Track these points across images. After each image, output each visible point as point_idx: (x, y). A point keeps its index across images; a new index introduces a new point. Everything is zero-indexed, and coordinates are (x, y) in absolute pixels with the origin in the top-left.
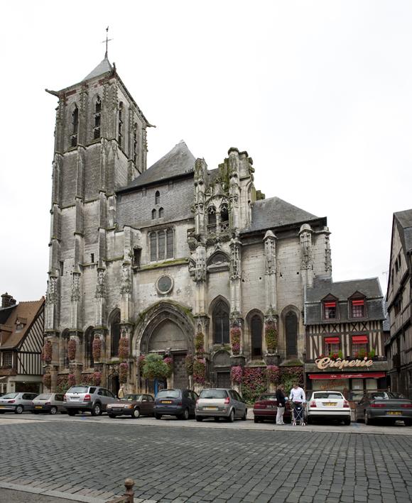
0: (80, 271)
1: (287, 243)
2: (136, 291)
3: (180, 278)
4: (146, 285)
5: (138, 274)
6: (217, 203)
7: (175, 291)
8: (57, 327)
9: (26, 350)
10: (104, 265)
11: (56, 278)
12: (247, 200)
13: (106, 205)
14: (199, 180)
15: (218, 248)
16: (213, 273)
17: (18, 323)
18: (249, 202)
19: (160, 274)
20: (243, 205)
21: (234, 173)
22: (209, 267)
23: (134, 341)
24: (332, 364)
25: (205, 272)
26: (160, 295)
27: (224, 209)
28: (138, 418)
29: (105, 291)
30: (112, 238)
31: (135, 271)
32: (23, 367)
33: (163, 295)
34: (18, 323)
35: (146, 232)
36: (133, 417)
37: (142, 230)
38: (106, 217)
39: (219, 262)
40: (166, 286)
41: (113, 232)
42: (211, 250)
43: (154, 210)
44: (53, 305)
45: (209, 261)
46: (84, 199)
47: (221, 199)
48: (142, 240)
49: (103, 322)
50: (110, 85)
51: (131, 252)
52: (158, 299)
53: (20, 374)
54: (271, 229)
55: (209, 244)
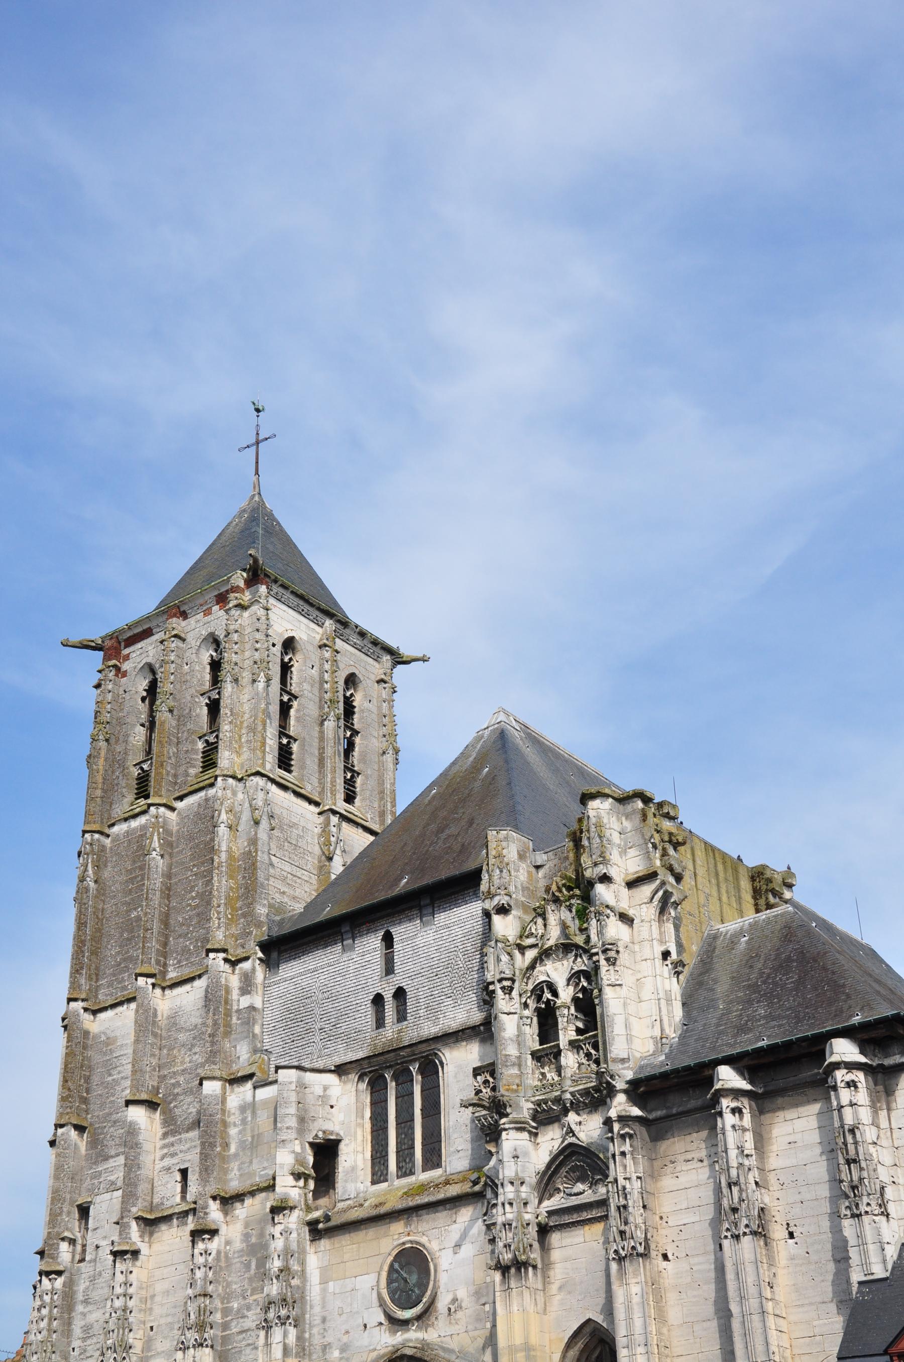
2: (314, 1313)
3: (455, 1250)
5: (324, 1243)
6: (557, 971)
7: (442, 1303)
11: (59, 1273)
12: (659, 949)
13: (228, 990)
14: (496, 900)
15: (571, 1132)
18: (666, 955)
19: (397, 1236)
22: (550, 1204)
25: (533, 1230)
27: (584, 990)
29: (218, 1317)
30: (243, 1109)
33: (405, 1324)
35: (354, 1077)
39: (580, 1187)
42: (551, 1140)
43: (378, 1000)
45: (547, 1183)
46: (164, 973)
48: (344, 1109)
54: (728, 1061)
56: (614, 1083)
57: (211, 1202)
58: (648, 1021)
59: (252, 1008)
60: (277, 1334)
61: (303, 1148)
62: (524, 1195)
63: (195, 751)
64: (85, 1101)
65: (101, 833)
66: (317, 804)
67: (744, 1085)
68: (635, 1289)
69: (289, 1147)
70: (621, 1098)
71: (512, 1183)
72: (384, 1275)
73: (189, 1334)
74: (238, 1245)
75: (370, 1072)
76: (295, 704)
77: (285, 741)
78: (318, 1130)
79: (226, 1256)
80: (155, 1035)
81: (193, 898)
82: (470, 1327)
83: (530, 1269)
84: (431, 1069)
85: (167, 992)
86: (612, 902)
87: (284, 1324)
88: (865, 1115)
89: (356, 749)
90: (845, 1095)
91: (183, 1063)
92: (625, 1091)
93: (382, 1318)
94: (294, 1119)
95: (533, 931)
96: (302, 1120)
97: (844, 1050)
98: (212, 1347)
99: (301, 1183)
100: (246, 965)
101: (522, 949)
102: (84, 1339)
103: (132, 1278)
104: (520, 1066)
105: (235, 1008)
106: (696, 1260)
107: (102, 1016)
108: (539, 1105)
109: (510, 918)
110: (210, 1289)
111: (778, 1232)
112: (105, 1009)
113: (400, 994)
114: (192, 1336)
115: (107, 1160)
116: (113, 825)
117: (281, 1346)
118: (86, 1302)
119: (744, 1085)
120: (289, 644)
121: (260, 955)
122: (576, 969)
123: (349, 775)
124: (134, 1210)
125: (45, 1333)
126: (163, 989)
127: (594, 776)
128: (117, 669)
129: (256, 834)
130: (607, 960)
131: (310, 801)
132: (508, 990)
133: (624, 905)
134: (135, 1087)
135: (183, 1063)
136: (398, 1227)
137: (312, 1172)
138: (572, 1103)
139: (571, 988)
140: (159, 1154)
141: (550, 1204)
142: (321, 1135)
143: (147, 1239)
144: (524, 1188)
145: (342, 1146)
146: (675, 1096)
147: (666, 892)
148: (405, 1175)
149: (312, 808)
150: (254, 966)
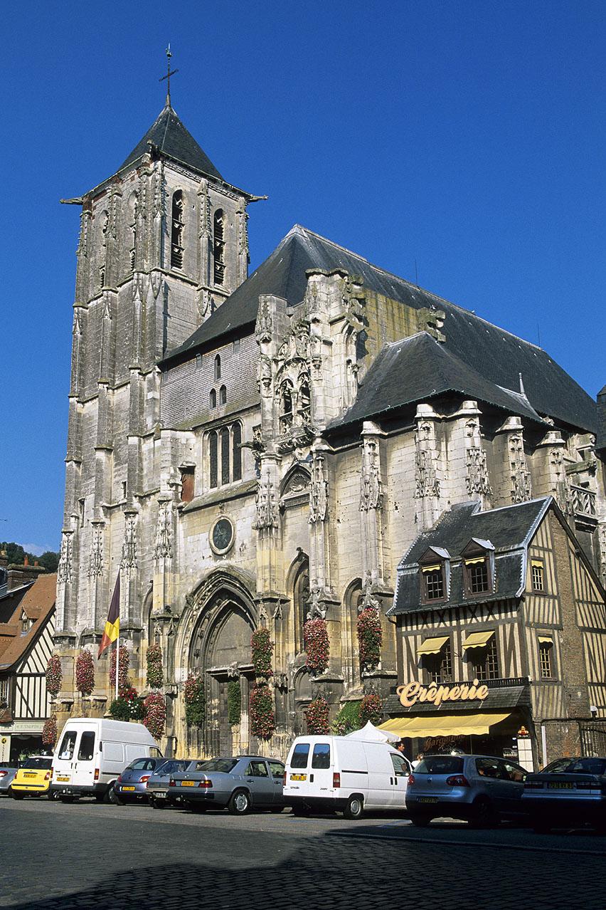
0: (104, 519)
1: (403, 441)
2: (181, 553)
3: (244, 519)
4: (196, 537)
6: (292, 373)
7: (237, 546)
8: (71, 627)
9: (34, 671)
10: (136, 503)
11: (71, 533)
12: (344, 360)
13: (141, 390)
15: (295, 459)
16: (291, 508)
17: (24, 618)
19: (215, 516)
20: (336, 370)
21: (311, 317)
22: (286, 496)
23: (178, 652)
24: (424, 696)
26: (217, 557)
27: (306, 383)
28: (247, 812)
30: (149, 451)
31: (183, 512)
32: (27, 703)
34: (24, 618)
36: (234, 812)
37: (195, 430)
38: (141, 413)
39: (300, 487)
40: (223, 534)
41: (152, 439)
42: (287, 464)
43: (213, 392)
44: (63, 586)
45: (285, 485)
46: (114, 382)
47: (300, 364)
48: (195, 448)
49: (130, 613)
50: (149, 175)
51: (173, 476)
52: (211, 565)
53: (21, 718)
54: (368, 419)
55: (285, 451)
56: (314, 433)
57: (134, 497)
58: (337, 398)
59: (154, 399)
60: (161, 562)
61: (175, 471)
62: (272, 492)
63: (128, 259)
64: (80, 449)
65: (84, 308)
66: (196, 285)
67: (378, 432)
68: (320, 537)
69: (167, 470)
70: (319, 440)
71: (266, 486)
72: (212, 533)
73: (124, 561)
74: (148, 519)
75: (210, 430)
76: (183, 228)
77: (176, 250)
78: (183, 462)
79: (143, 525)
80: (109, 414)
81: (127, 341)
82: (250, 557)
83: (274, 529)
84: (237, 426)
85: (115, 391)
86: (320, 334)
87: (165, 557)
88: (432, 445)
89: (224, 252)
90: (422, 434)
91: (123, 428)
92: (321, 437)
93: (211, 553)
94: (170, 456)
95: (283, 352)
96: (174, 456)
97: (425, 410)
98: (136, 567)
99: (174, 488)
100: (150, 376)
101: (276, 362)
102: (85, 563)
103: (102, 535)
104: (273, 425)
105: (145, 399)
106: (352, 522)
107: (86, 405)
108: (282, 446)
109: (270, 344)
110: (135, 540)
111: (391, 507)
112: (88, 401)
113: (223, 388)
114: (126, 562)
115: (91, 478)
116: (89, 303)
117: (163, 567)
118: (84, 546)
119: (378, 432)
120: (178, 195)
121: (158, 370)
122: (302, 372)
123: (219, 268)
124: (101, 502)
125: (66, 560)
126: (113, 390)
127: (359, 261)
128: (90, 214)
129: (155, 304)
130: (315, 366)
131: (192, 284)
132: (268, 385)
133: (327, 336)
134: (100, 441)
135: (123, 428)
136: (217, 509)
137: (181, 483)
138: (297, 444)
139: (300, 382)
140: (113, 475)
141: (286, 496)
142: (184, 464)
143: (108, 517)
144: (272, 489)
145: (196, 469)
146: (344, 435)
147: (350, 326)
148: (226, 483)
149: (193, 287)
150: (154, 374)
